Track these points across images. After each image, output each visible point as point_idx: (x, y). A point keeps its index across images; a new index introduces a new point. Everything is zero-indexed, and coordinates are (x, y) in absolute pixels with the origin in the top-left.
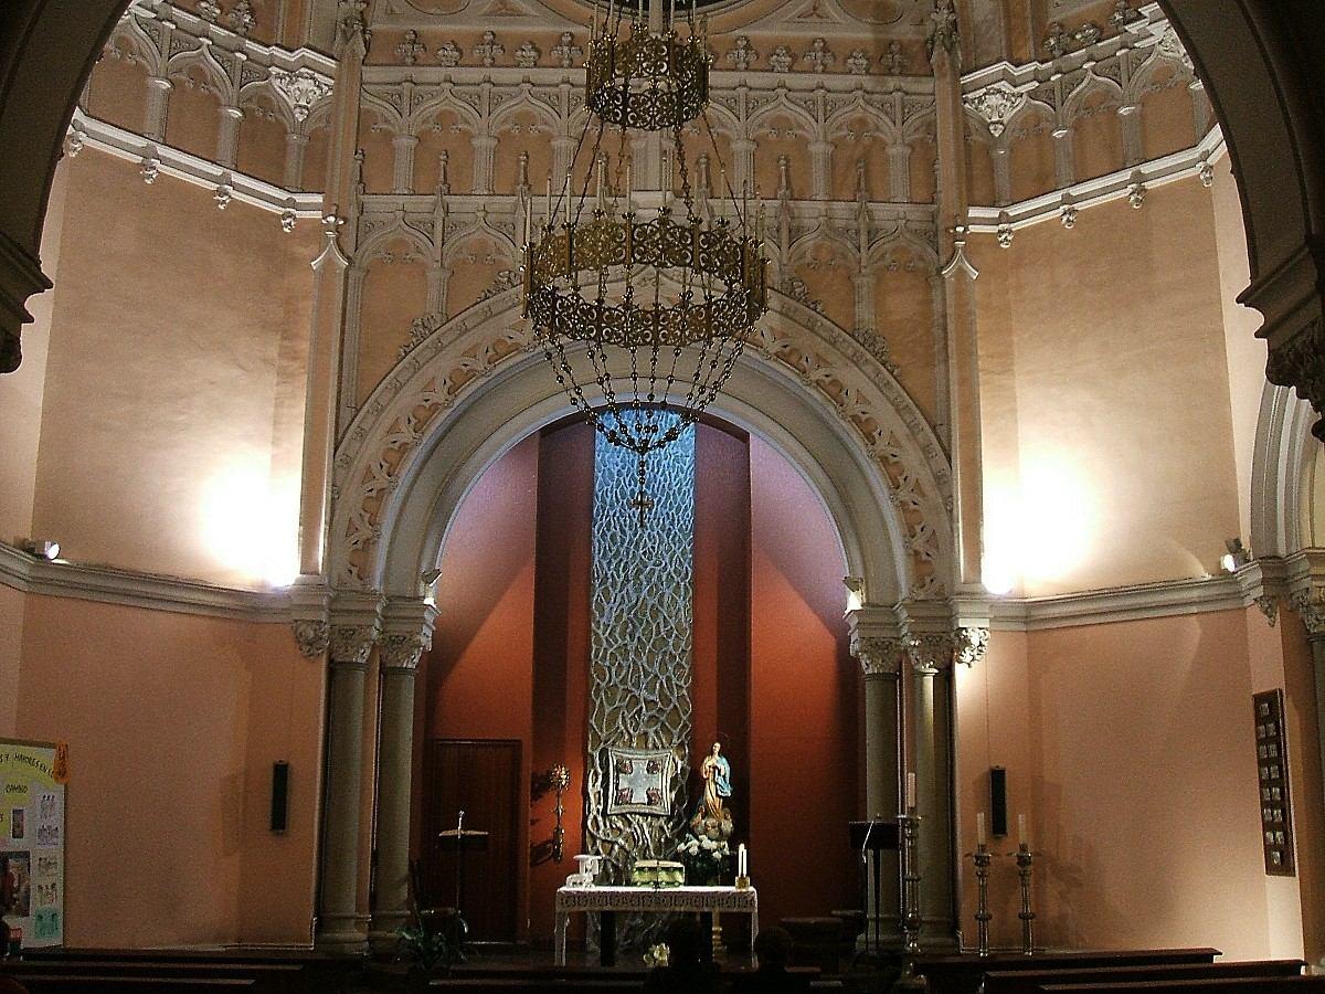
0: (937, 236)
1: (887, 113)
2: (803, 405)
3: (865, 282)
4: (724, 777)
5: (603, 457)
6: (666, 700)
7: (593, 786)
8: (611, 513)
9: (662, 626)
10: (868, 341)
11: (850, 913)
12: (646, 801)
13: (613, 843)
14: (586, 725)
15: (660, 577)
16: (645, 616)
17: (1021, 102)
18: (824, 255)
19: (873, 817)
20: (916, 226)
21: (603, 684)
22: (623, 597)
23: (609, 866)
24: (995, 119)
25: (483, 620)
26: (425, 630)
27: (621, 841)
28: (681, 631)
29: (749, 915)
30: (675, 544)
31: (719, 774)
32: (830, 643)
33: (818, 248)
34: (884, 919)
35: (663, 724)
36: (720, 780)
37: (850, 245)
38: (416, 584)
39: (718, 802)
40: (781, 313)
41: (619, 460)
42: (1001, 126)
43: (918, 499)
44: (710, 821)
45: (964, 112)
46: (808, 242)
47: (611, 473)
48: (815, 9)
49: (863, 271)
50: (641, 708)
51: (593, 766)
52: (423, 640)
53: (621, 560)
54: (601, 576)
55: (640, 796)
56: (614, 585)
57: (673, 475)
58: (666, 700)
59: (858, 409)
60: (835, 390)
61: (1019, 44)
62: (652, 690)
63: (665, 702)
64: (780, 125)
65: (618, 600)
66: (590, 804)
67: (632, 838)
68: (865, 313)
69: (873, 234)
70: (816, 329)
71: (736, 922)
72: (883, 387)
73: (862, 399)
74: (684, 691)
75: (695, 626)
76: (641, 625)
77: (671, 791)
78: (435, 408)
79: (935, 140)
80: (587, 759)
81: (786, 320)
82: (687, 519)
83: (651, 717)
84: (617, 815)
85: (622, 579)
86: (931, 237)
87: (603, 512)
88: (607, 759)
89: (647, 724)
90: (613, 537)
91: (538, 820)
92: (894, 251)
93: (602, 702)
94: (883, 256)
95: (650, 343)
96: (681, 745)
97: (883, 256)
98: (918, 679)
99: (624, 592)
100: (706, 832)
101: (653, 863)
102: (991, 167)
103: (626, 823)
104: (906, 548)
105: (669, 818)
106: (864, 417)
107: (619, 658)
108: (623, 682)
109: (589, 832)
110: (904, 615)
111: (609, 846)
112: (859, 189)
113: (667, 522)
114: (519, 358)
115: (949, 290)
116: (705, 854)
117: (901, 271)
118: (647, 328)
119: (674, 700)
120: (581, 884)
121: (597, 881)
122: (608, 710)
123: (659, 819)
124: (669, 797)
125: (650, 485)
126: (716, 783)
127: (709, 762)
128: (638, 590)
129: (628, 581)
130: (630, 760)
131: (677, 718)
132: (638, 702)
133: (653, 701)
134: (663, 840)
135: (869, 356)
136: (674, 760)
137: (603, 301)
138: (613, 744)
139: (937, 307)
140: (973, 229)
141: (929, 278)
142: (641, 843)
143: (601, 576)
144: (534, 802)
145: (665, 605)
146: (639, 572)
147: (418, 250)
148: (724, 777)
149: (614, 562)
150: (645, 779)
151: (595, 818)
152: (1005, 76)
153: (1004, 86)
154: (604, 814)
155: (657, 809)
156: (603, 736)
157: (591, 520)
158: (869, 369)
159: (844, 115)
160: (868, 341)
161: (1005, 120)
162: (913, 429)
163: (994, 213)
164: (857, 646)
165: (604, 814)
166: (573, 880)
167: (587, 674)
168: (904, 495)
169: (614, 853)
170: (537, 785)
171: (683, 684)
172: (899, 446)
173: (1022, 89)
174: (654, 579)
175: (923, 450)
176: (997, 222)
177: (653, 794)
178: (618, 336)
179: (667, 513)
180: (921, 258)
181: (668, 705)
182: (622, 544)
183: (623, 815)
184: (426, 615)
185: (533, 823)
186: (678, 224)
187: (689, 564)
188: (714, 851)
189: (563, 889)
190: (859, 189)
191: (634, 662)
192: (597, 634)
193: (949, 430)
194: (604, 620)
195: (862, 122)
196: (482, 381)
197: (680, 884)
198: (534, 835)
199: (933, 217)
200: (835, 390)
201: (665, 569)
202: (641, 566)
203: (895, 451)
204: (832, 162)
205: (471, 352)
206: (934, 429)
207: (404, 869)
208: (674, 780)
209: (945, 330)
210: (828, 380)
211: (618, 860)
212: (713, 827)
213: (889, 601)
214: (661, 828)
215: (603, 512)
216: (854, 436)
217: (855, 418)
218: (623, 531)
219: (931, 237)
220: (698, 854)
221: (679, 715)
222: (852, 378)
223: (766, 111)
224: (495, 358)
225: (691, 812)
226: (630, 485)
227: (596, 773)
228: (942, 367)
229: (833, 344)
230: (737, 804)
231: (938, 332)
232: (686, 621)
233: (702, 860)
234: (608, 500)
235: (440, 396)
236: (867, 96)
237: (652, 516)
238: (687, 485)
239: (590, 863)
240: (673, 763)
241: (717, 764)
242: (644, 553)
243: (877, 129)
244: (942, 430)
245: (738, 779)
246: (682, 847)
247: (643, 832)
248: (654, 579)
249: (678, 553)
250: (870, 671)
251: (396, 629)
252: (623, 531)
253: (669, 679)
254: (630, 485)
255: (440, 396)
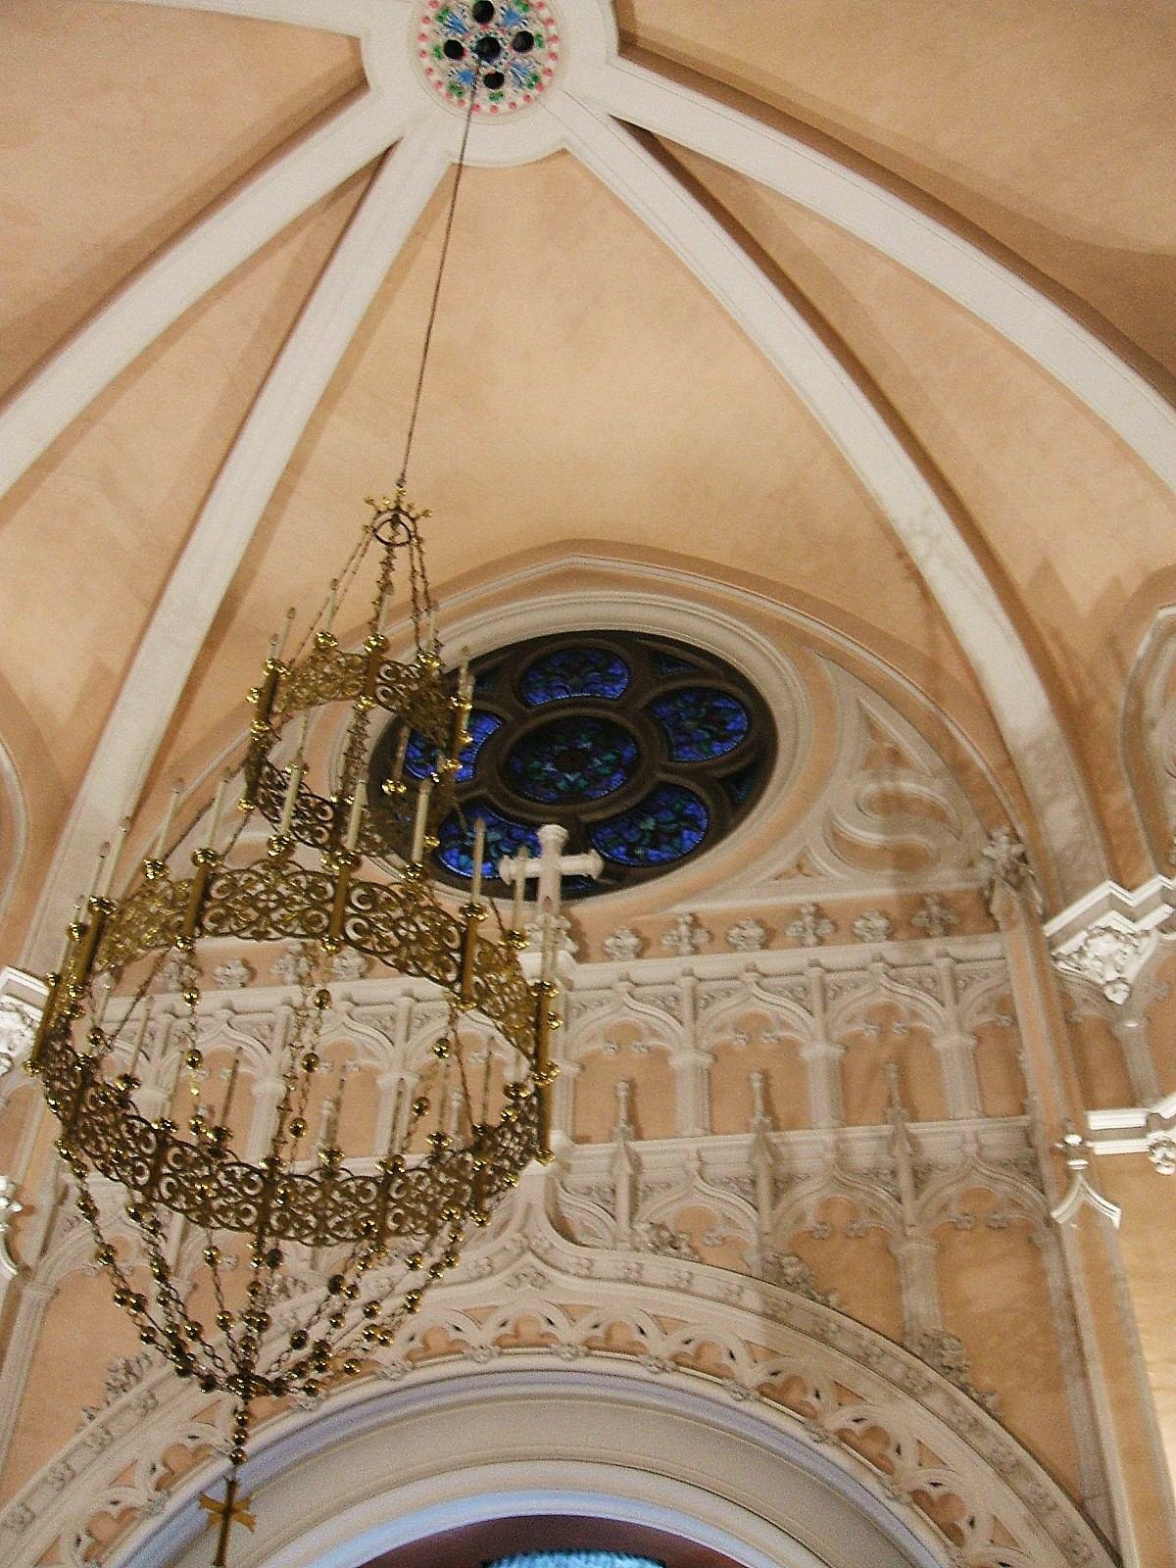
0: (1036, 1163)
1: (928, 991)
3: (915, 1249)
10: (929, 1349)
17: (1148, 946)
18: (839, 1217)
20: (996, 1154)
24: (1111, 975)
33: (827, 1205)
37: (883, 1195)
40: (764, 1315)
42: (1125, 987)
45: (1060, 978)
46: (808, 1197)
48: (799, 867)
59: (921, 1479)
60: (873, 1446)
61: (1129, 869)
64: (752, 1026)
69: (921, 1175)
70: (830, 1336)
72: (966, 1431)
73: (927, 1456)
78: (128, 1516)
79: (1015, 1021)
86: (1030, 1169)
92: (966, 1196)
94: (945, 1208)
97: (945, 1208)
102: (1118, 1052)
112: (890, 1104)
115: (1070, 1243)
117: (981, 1229)
135: (932, 1375)
137: (280, 1163)
139: (1054, 1281)
140: (1101, 1148)
141: (1034, 1236)
152: (1113, 903)
153: (1114, 919)
158: (936, 1400)
159: (857, 1001)
160: (929, 1349)
161: (1130, 974)
162: (1038, 1511)
163: (1134, 1118)
172: (1013, 1542)
173: (1149, 922)
176: (1140, 1132)
178: (230, 1176)
180: (1015, 1204)
186: (307, 869)
190: (890, 1104)
193: (1111, 1510)
195: (890, 1010)
199: (1027, 1134)
200: (873, 1447)
204: (841, 1073)
206: (1080, 1506)
209: (1074, 1320)
216: (922, 1532)
217: (918, 1497)
219: (1030, 1169)
223: (727, 1009)
228: (1080, 1384)
229: (866, 1363)
231: (1061, 1325)
235: (139, 1494)
236: (893, 972)
243: (914, 1015)
244: (1097, 1508)
255: (139, 1494)
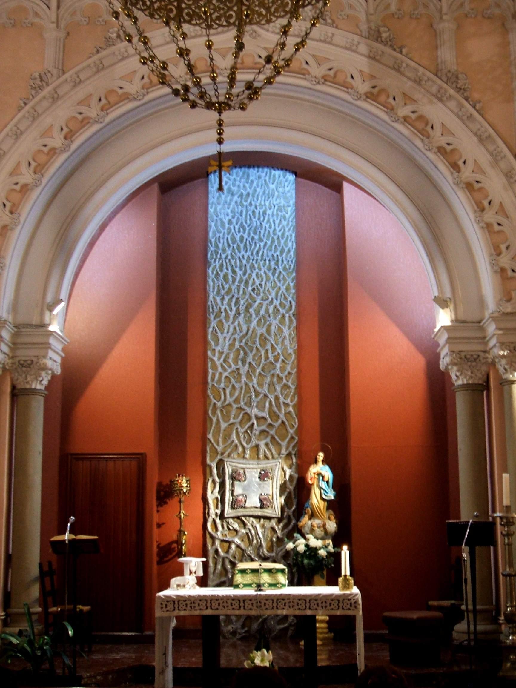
2: (392, 145)
3: (446, 26)
4: (328, 482)
5: (216, 209)
6: (274, 415)
7: (212, 492)
8: (224, 256)
9: (270, 351)
11: (446, 603)
12: (259, 505)
13: (230, 543)
14: (204, 440)
15: (267, 310)
16: (254, 343)
19: (467, 514)
21: (219, 404)
22: (235, 328)
23: (227, 562)
25: (111, 349)
26: (51, 354)
27: (237, 540)
28: (287, 356)
29: (352, 619)
30: (280, 281)
31: (323, 480)
32: (419, 362)
34: (481, 611)
35: (273, 438)
36: (323, 485)
38: (42, 314)
39: (322, 505)
40: (369, 57)
41: (229, 211)
43: (502, 220)
44: (316, 522)
47: (223, 223)
49: (444, 17)
50: (253, 424)
51: (211, 475)
52: (49, 363)
53: (233, 296)
54: (215, 310)
55: (253, 501)
56: (227, 317)
57: (277, 222)
58: (274, 415)
59: (443, 141)
60: (421, 125)
62: (261, 407)
63: (274, 418)
65: (231, 330)
66: (209, 508)
67: (248, 537)
68: (447, 55)
71: (342, 627)
73: (446, 131)
74: (291, 409)
75: (299, 352)
76: (251, 351)
77: (281, 496)
78: (53, 152)
80: (205, 466)
81: (377, 64)
82: (289, 258)
83: (262, 432)
84: (233, 518)
85: (234, 312)
87: (216, 256)
88: (224, 469)
89: (259, 438)
90: (225, 277)
91: (163, 524)
93: (218, 420)
95: (234, 24)
96: (289, 455)
98: (506, 387)
99: (236, 324)
100: (312, 531)
101: (255, 565)
103: (242, 525)
104: (492, 265)
105: (280, 520)
106: (449, 148)
107: (233, 380)
108: (237, 401)
109: (209, 533)
110: (491, 328)
111: (226, 545)
113: (273, 263)
114: (130, 105)
116: (311, 551)
118: (230, 9)
119: (282, 416)
120: (184, 586)
121: (202, 582)
122: (224, 425)
123: (270, 521)
124: (279, 501)
125: (255, 218)
126: (320, 488)
127: (313, 470)
128: (248, 321)
129: (239, 314)
130: (244, 469)
131: (284, 431)
132: (250, 419)
133: (263, 418)
134: (274, 539)
135: (452, 92)
136: (283, 468)
138: (229, 456)
142: (255, 541)
143: (216, 310)
144: (160, 508)
145: (273, 334)
146: (248, 307)
147: (36, 14)
148: (328, 482)
149: (227, 298)
150: (257, 485)
151: (214, 521)
154: (222, 517)
155: (268, 512)
156: (220, 448)
157: (206, 263)
158: (452, 104)
160: (452, 79)
164: (447, 360)
165: (222, 517)
166: (178, 583)
167: (205, 396)
168: (490, 216)
169: (231, 551)
170: (162, 493)
171: (290, 402)
172: (483, 173)
174: (262, 312)
175: (506, 175)
177: (265, 499)
179: (273, 255)
181: (277, 421)
182: (234, 282)
183: (238, 518)
184: (52, 341)
185: (159, 526)
187: (293, 298)
188: (320, 549)
189: (162, 594)
191: (246, 384)
192: (212, 360)
194: (218, 348)
196: (95, 128)
197: (283, 585)
198: (157, 538)
200: (420, 125)
201: (271, 302)
202: (250, 301)
203: (479, 177)
205: (85, 101)
207: (35, 571)
208: (283, 488)
210: (413, 116)
211: (235, 557)
212: (319, 527)
213: (476, 318)
214: (273, 529)
215: (216, 256)
218: (234, 272)
220: (305, 552)
221: (287, 430)
222: (438, 113)
224: (107, 107)
225: (299, 513)
226: (239, 232)
227: (214, 482)
230: (340, 506)
232: (291, 348)
233: (309, 557)
234: (220, 245)
237: (259, 258)
238: (289, 230)
239: (194, 564)
240: (281, 471)
241: (321, 472)
242: (253, 290)
245: (341, 484)
246: (290, 545)
247: (257, 533)
248: (262, 312)
249: (283, 289)
250: (460, 382)
251: (24, 354)
252: (234, 272)
253: (277, 398)
254: (239, 232)
